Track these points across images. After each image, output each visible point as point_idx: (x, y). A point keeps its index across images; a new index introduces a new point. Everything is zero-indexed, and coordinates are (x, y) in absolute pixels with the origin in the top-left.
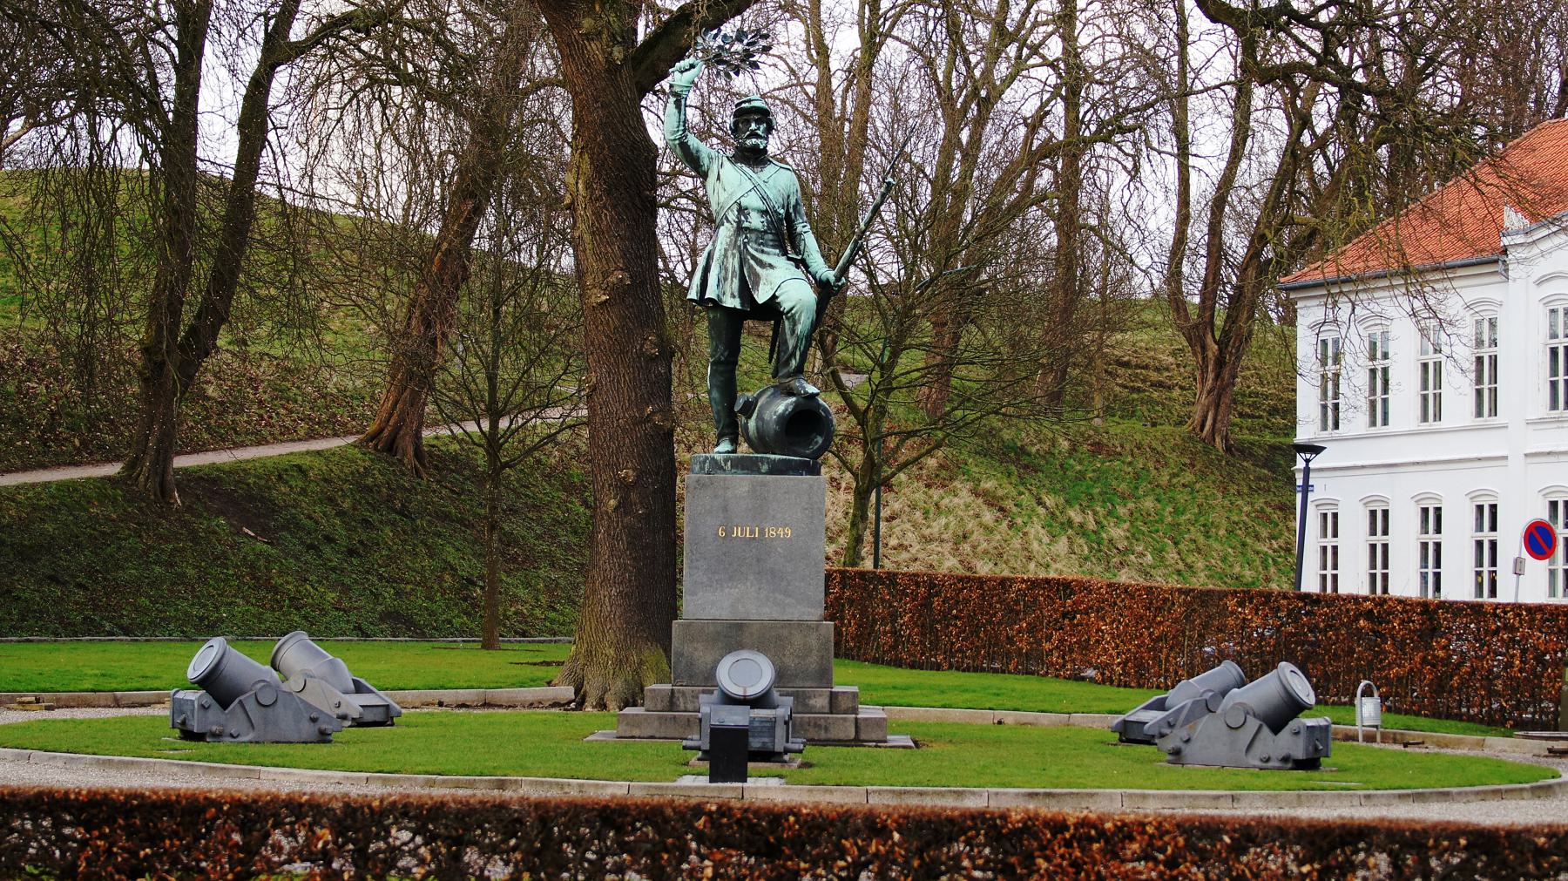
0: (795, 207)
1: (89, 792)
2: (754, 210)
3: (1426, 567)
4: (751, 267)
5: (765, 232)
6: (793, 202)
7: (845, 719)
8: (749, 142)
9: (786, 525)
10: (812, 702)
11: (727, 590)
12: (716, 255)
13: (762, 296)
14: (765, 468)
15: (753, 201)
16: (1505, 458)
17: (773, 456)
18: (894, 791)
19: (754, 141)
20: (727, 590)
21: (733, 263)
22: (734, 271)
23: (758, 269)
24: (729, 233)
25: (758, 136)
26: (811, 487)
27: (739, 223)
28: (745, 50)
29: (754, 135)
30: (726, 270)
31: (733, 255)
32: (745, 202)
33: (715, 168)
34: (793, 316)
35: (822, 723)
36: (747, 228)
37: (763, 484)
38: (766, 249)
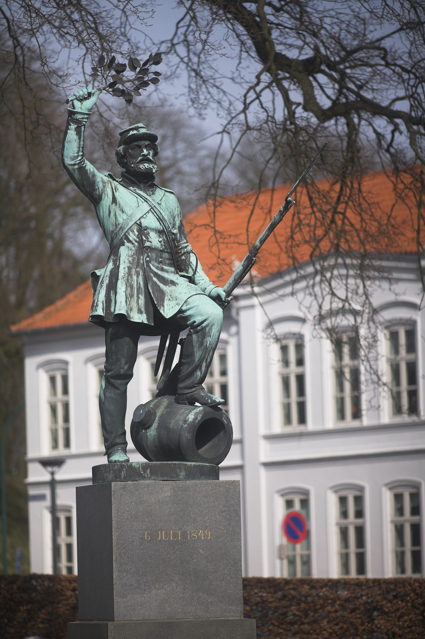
2: (152, 230)
12: (122, 272)
17: (189, 463)
22: (139, 289)
23: (162, 286)
24: (131, 253)
25: (149, 161)
27: (141, 242)
28: (137, 79)
29: (146, 160)
30: (132, 287)
31: (138, 274)
32: (145, 223)
33: (109, 191)
34: (204, 328)
38: (165, 267)
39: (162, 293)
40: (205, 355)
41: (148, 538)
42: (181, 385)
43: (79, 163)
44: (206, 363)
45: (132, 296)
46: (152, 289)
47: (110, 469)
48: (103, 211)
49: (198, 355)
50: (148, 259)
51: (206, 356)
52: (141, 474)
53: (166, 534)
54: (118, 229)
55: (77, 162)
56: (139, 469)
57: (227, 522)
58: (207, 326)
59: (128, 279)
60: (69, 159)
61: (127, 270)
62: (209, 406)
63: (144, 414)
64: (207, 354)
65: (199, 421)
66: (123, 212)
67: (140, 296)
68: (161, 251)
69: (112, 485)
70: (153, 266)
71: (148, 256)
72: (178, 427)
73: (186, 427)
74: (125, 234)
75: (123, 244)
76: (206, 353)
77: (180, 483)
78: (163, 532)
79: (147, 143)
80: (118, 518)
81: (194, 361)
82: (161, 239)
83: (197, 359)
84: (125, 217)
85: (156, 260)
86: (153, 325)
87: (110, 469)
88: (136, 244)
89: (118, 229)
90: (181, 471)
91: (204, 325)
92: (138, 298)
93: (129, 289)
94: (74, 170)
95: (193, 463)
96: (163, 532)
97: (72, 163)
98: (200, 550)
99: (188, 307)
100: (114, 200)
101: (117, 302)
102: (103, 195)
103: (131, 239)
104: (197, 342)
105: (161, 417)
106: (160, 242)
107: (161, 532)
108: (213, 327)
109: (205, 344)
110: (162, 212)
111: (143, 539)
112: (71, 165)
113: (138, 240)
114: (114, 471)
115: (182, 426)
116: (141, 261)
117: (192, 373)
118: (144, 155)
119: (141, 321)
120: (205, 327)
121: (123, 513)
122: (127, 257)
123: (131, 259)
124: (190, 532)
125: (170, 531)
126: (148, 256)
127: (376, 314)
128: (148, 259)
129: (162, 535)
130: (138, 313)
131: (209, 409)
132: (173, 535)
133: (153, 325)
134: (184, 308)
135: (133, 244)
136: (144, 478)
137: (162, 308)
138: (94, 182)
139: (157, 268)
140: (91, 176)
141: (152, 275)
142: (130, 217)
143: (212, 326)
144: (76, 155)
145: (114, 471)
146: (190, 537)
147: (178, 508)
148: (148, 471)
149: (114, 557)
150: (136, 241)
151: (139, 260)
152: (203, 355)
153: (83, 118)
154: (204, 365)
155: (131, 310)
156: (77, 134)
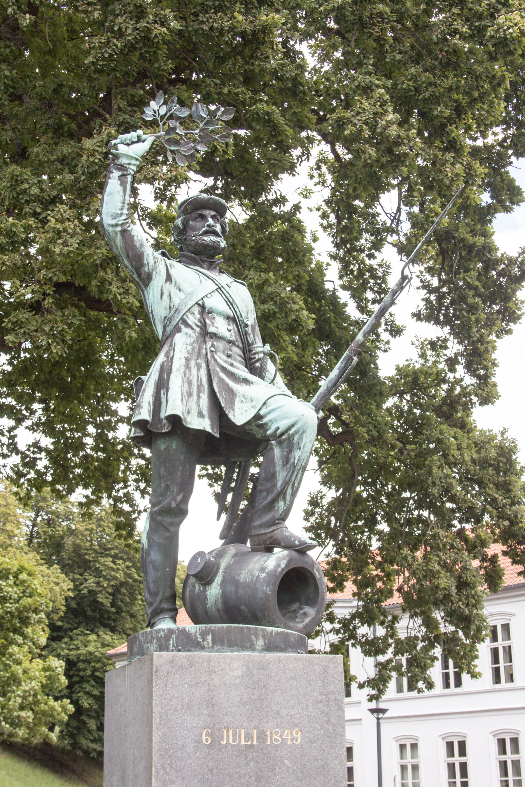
1: (429, 322)
2: (219, 314)
3: (454, 777)
4: (221, 381)
9: (295, 725)
14: (260, 643)
16: (360, 720)
17: (269, 629)
23: (232, 384)
24: (190, 340)
25: (216, 234)
26: (325, 670)
27: (204, 326)
30: (190, 383)
31: (199, 366)
32: (209, 303)
37: (263, 666)
39: (232, 393)
40: (291, 477)
41: (207, 740)
42: (257, 523)
43: (122, 224)
44: (293, 488)
45: (190, 394)
47: (152, 637)
48: (153, 295)
49: (281, 477)
50: (213, 349)
51: (293, 478)
52: (199, 643)
53: (234, 735)
54: (173, 312)
55: (120, 222)
56: (196, 636)
57: (325, 719)
58: (296, 432)
59: (185, 374)
60: (109, 218)
61: (183, 361)
62: (296, 550)
63: (203, 563)
64: (295, 474)
65: (283, 570)
66: (180, 290)
67: (201, 395)
69: (154, 657)
71: (213, 346)
72: (252, 579)
73: (264, 578)
74: (182, 318)
75: (179, 330)
76: (292, 474)
78: (231, 731)
79: (213, 213)
80: (162, 708)
81: (275, 486)
83: (279, 484)
84: (182, 295)
85: (223, 352)
86: (218, 436)
87: (152, 637)
88: (198, 329)
89: (173, 312)
90: (257, 639)
91: (291, 432)
92: (199, 397)
93: (186, 385)
94: (116, 233)
95: (275, 629)
96: (231, 731)
97: (114, 222)
98: (286, 762)
99: (268, 409)
100: (169, 278)
101: (169, 400)
102: (154, 273)
103: (190, 322)
104: (281, 457)
105: (226, 568)
107: (228, 731)
108: (305, 435)
109: (291, 461)
111: (199, 741)
112: (112, 226)
113: (199, 324)
114: (158, 639)
115: (258, 576)
116: (204, 351)
117: (271, 505)
118: (209, 226)
119: (202, 428)
120: (293, 435)
121: (171, 700)
122: (185, 346)
123: (189, 348)
124: (271, 733)
125: (240, 731)
127: (345, 619)
128: (213, 349)
129: (228, 736)
130: (198, 416)
131: (294, 554)
132: (245, 737)
133: (218, 436)
134: (262, 413)
135: (193, 329)
136: (203, 648)
137: (232, 412)
139: (226, 362)
140: (138, 245)
141: (218, 369)
142: (189, 295)
143: (302, 434)
144: (119, 212)
145: (158, 639)
146: (271, 739)
147: (254, 694)
148: (210, 637)
149: (154, 770)
150: (197, 326)
151: (200, 349)
152: (289, 476)
153: (129, 164)
154: (289, 491)
155: (189, 413)
156: (121, 184)
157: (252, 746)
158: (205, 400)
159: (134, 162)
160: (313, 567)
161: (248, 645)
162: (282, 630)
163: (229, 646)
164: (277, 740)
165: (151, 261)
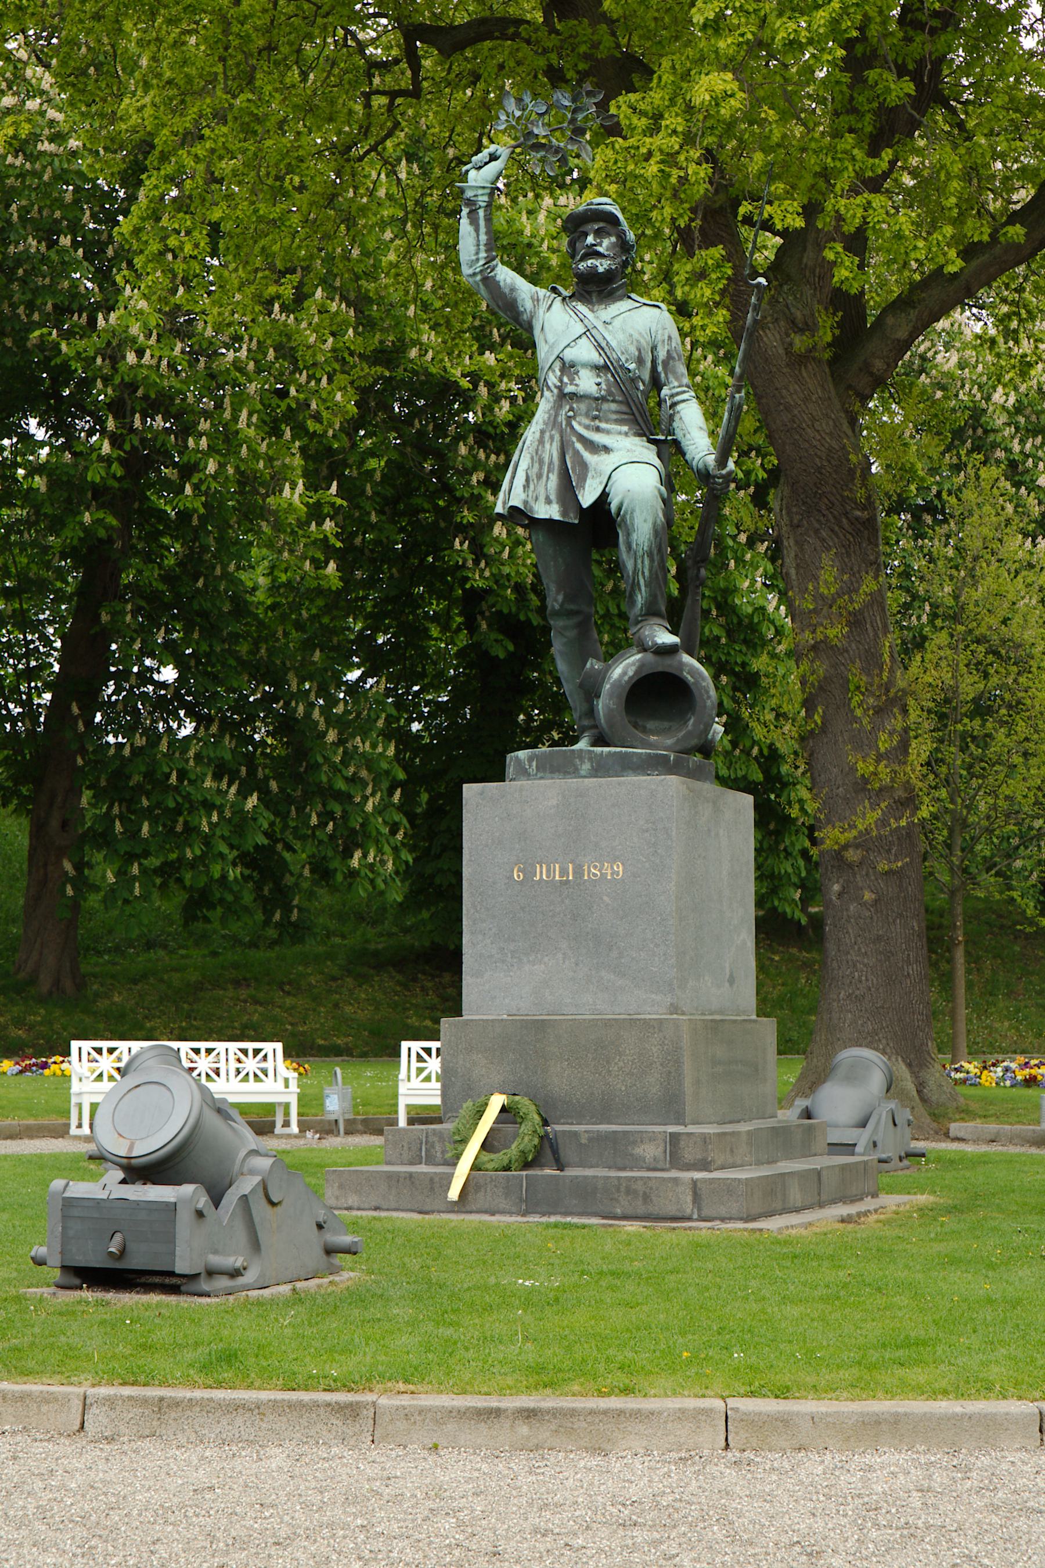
0: (665, 363)
2: (585, 365)
4: (577, 453)
5: (603, 399)
6: (662, 354)
7: (676, 1181)
8: (582, 266)
10: (638, 1151)
11: (527, 968)
13: (587, 497)
14: (586, 767)
15: (585, 352)
18: (145, 1401)
19: (589, 262)
20: (527, 968)
21: (551, 450)
22: (551, 463)
23: (587, 455)
24: (549, 406)
27: (560, 389)
32: (569, 355)
35: (639, 1187)
36: (573, 396)
38: (603, 425)
39: (584, 466)
46: (572, 462)
50: (571, 414)
53: (548, 871)
61: (538, 435)
65: (631, 678)
68: (597, 399)
70: (580, 424)
71: (571, 409)
77: (573, 782)
82: (599, 380)
85: (587, 415)
88: (556, 391)
90: (582, 762)
93: (536, 465)
98: (605, 898)
106: (598, 384)
110: (609, 338)
119: (547, 517)
126: (571, 409)
128: (571, 414)
131: (650, 657)
138: (515, 300)
139: (587, 427)
140: (507, 291)
141: (574, 439)
155: (537, 499)
156: (471, 223)
157: (568, 882)
158: (553, 481)
159: (480, 192)
160: (682, 670)
161: (571, 770)
162: (618, 749)
163: (552, 772)
164: (595, 875)
165: (529, 305)
